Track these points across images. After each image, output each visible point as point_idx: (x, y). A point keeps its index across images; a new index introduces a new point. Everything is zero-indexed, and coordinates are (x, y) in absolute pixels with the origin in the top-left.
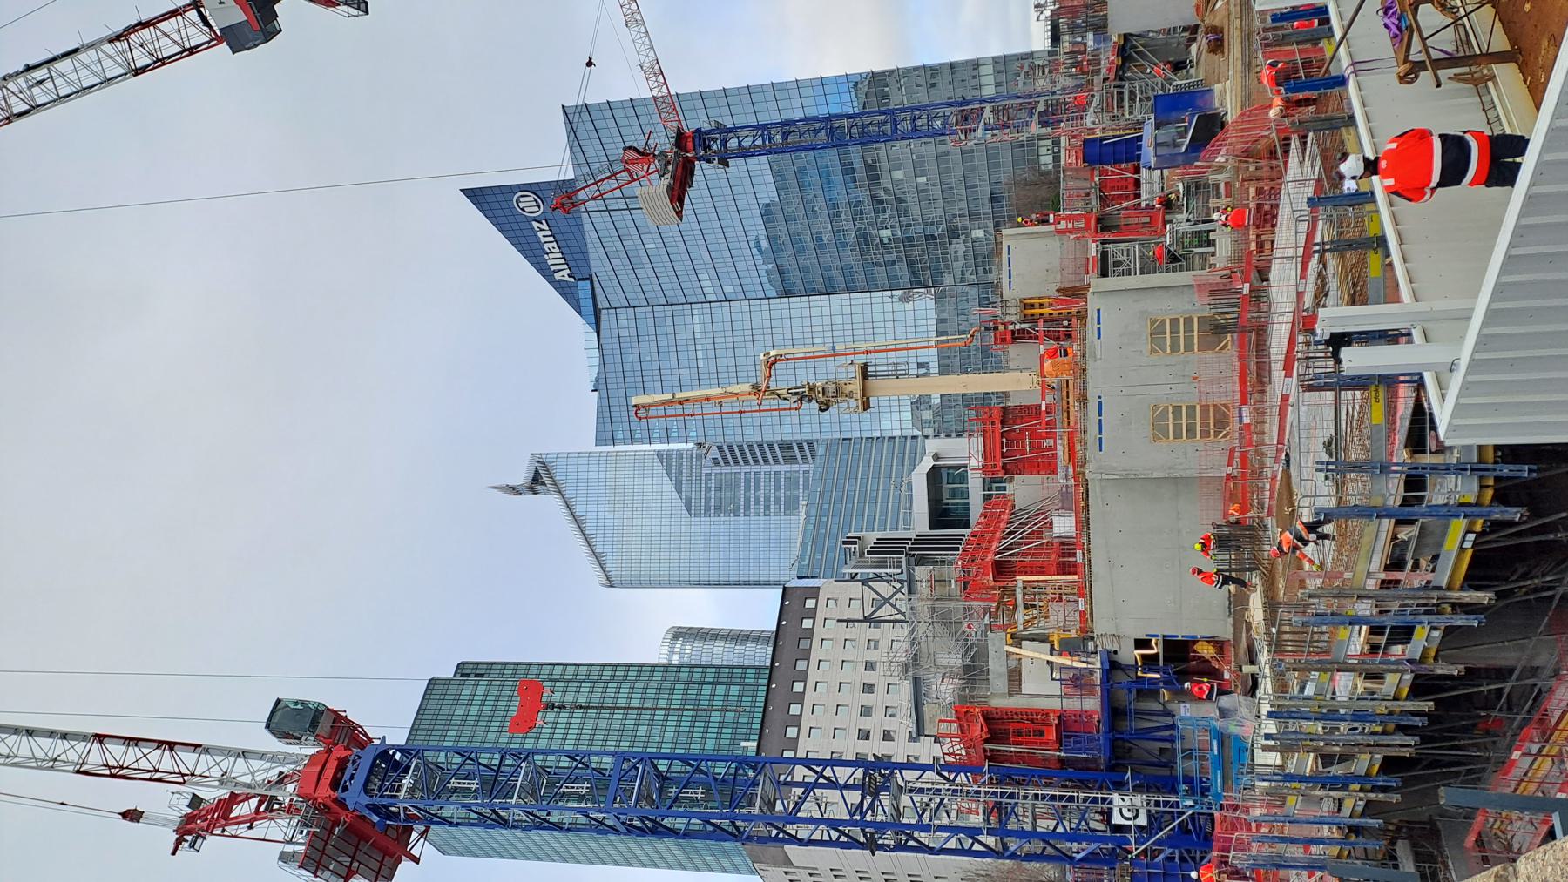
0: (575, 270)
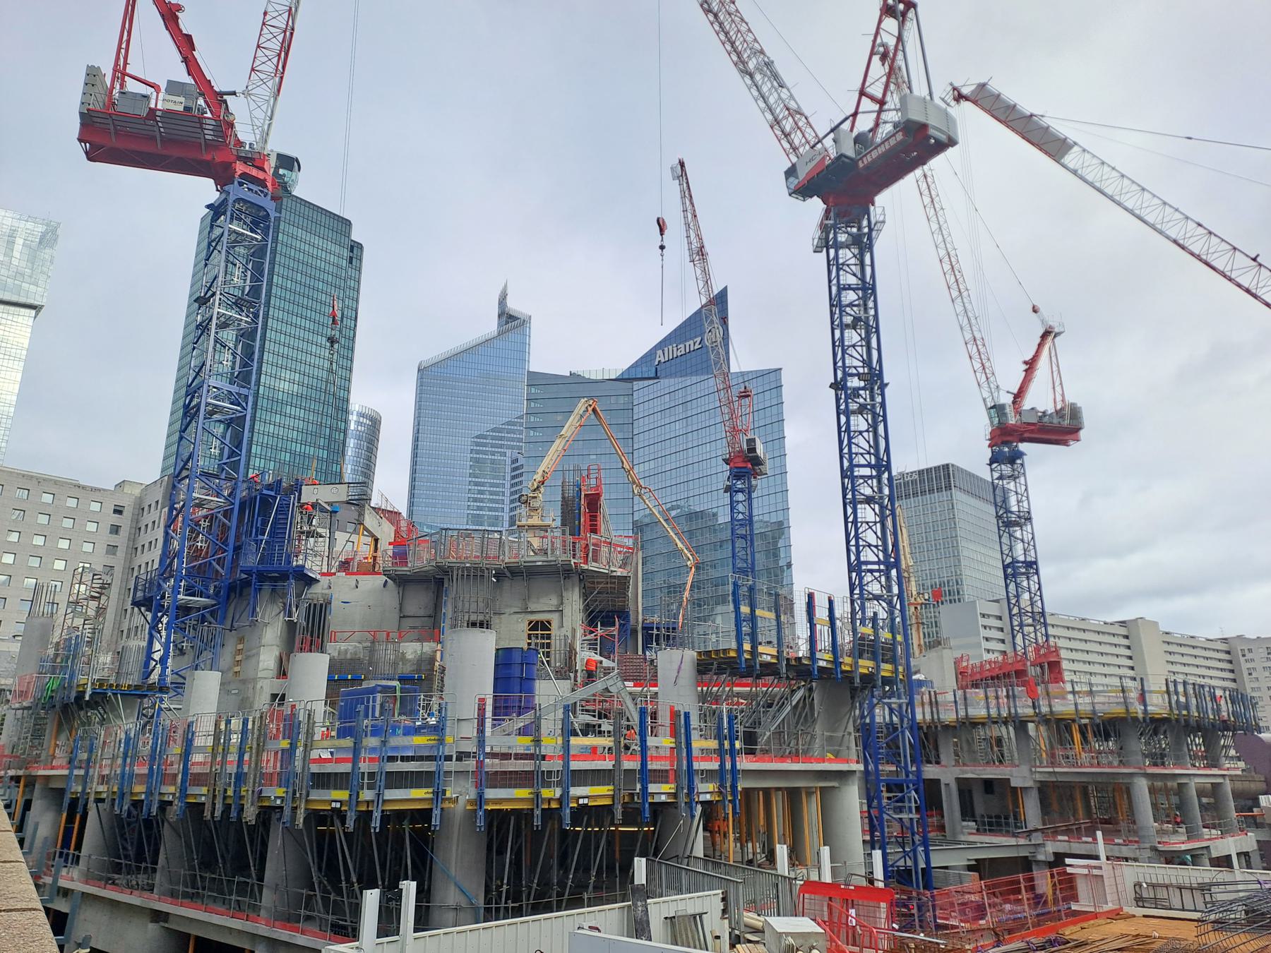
0: (663, 366)
